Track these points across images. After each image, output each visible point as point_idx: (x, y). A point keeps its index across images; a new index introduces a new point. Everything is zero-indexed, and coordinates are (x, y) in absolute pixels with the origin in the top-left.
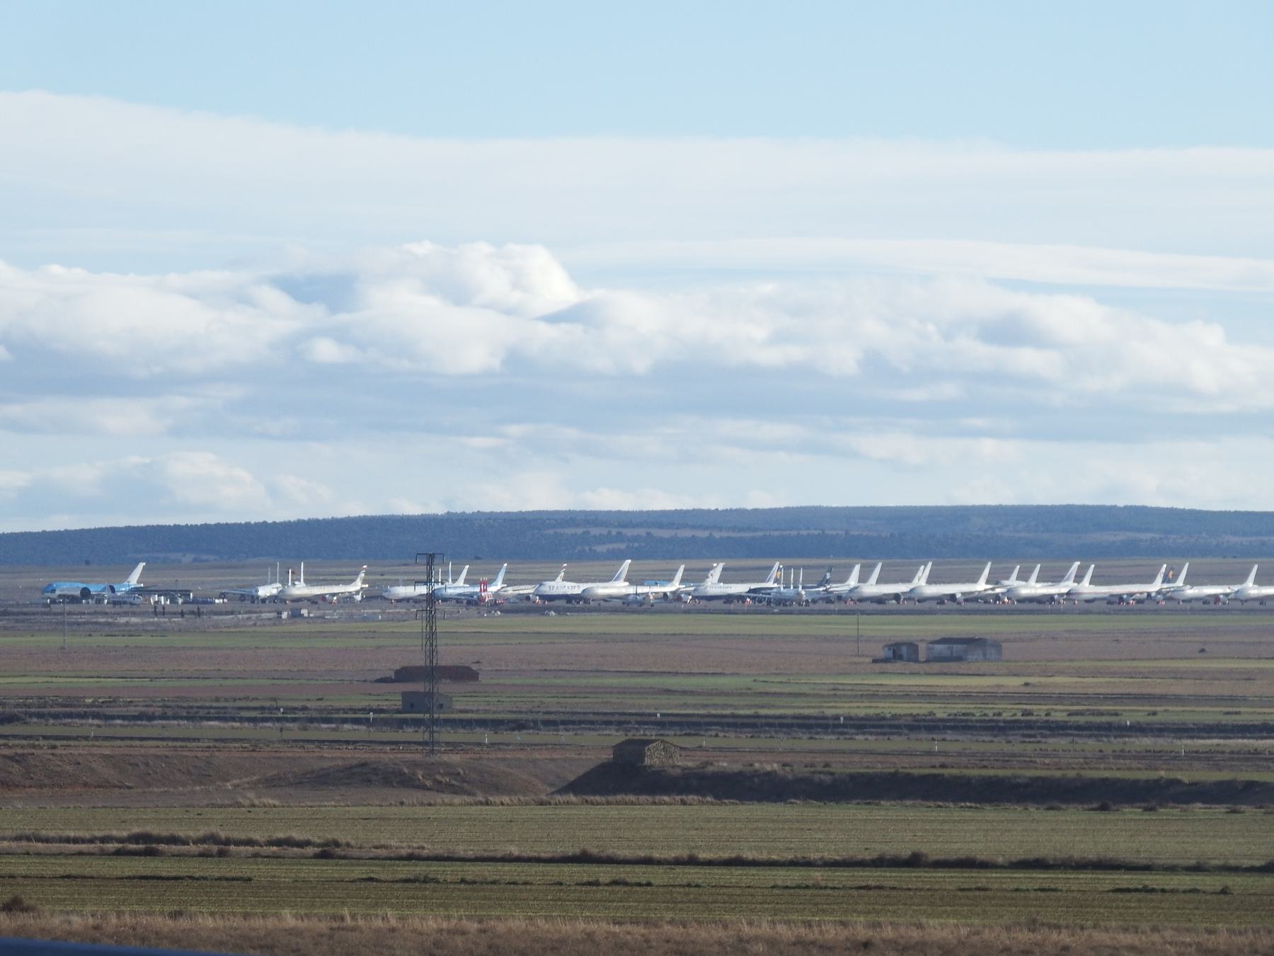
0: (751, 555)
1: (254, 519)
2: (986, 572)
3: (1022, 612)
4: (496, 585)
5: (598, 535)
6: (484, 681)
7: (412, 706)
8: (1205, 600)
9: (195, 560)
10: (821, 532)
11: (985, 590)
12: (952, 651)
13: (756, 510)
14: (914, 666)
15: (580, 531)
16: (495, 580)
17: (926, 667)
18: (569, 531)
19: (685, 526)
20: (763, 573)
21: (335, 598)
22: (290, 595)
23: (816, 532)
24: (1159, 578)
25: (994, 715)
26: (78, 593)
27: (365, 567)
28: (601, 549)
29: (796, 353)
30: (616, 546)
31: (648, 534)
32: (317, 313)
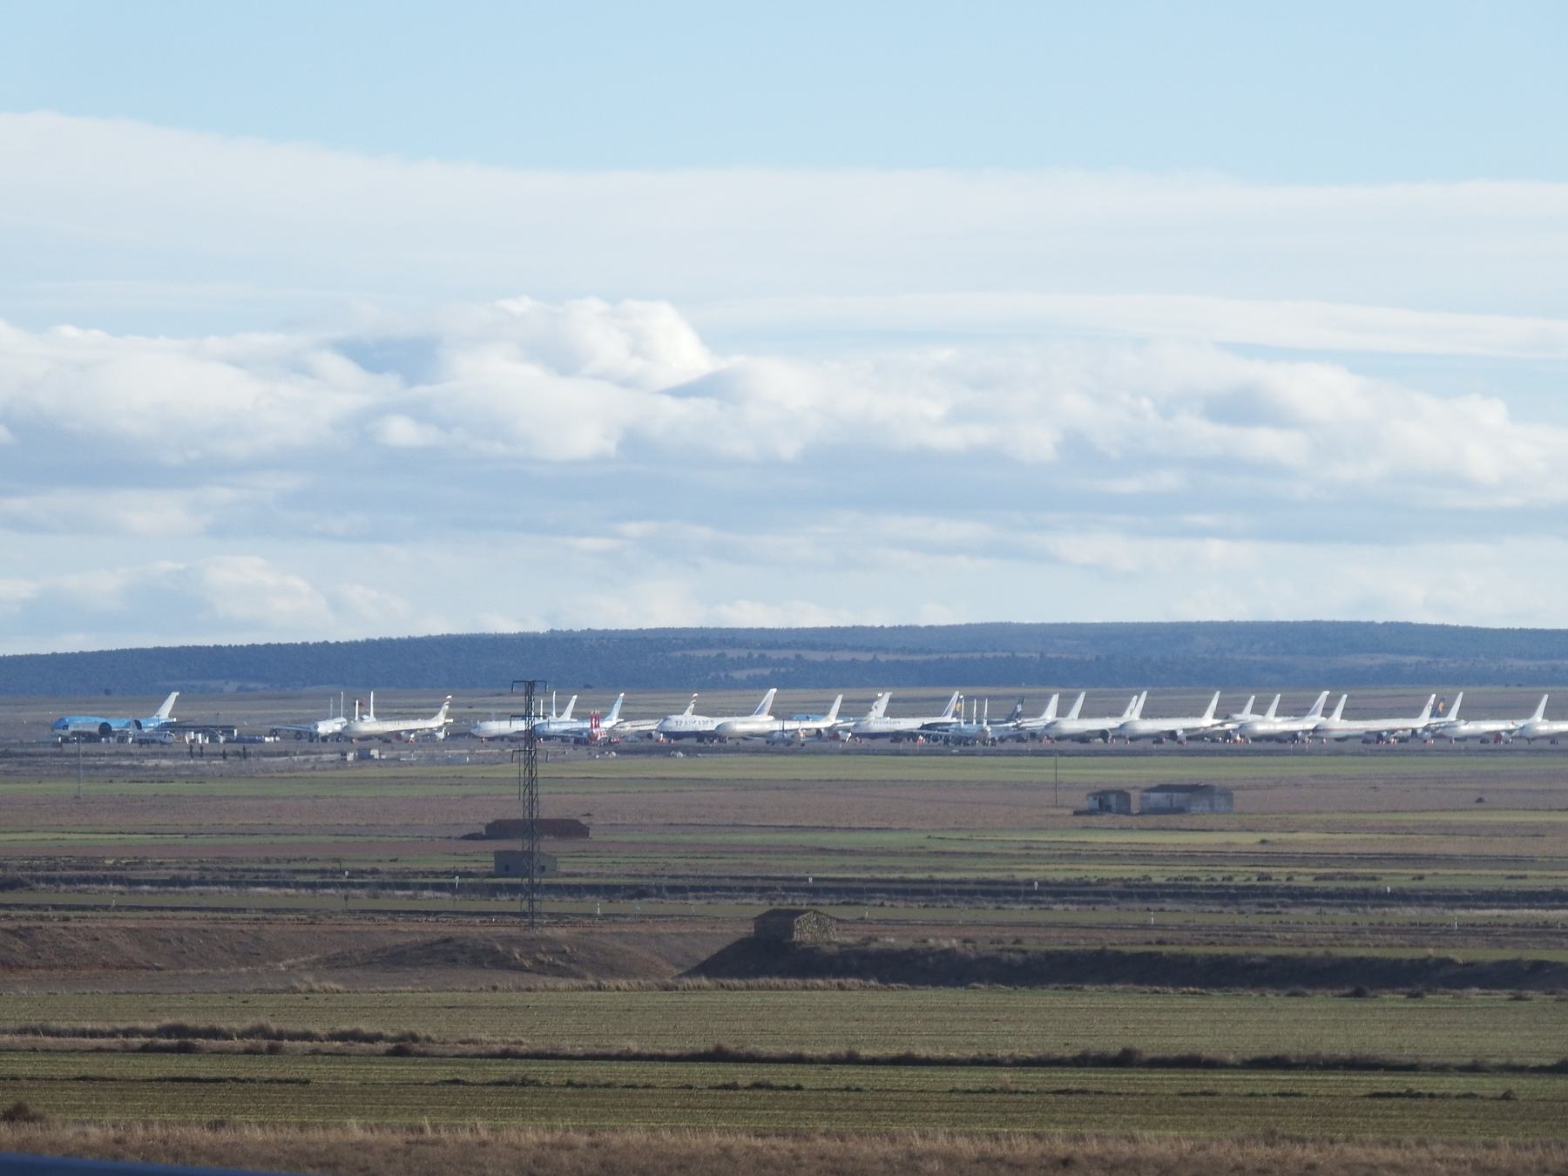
0: (924, 683)
1: (313, 638)
2: (1214, 703)
3: (1257, 753)
4: (611, 720)
5: (736, 658)
6: (596, 838)
7: (507, 868)
8: (1483, 738)
9: (240, 689)
10: (1010, 654)
11: (1213, 726)
12: (1171, 801)
13: (930, 628)
14: (1125, 820)
15: (713, 653)
16: (609, 713)
17: (1140, 821)
18: (701, 653)
19: (843, 647)
20: (939, 705)
21: (412, 736)
22: (356, 732)
23: (1004, 655)
24: (1427, 711)
25: (1223, 879)
26: (96, 730)
27: (449, 697)
28: (740, 675)
29: (979, 434)
30: (758, 671)
31: (798, 657)
32: (390, 385)
